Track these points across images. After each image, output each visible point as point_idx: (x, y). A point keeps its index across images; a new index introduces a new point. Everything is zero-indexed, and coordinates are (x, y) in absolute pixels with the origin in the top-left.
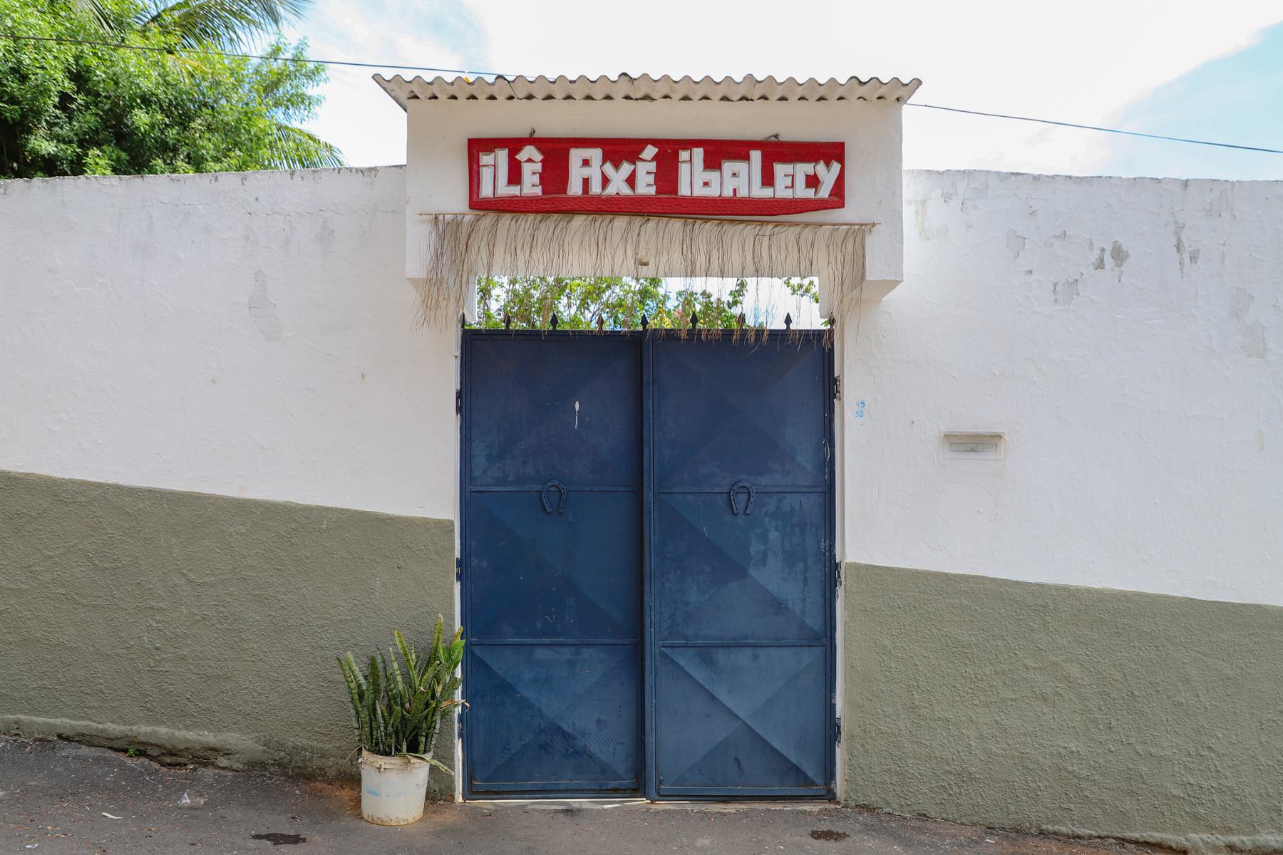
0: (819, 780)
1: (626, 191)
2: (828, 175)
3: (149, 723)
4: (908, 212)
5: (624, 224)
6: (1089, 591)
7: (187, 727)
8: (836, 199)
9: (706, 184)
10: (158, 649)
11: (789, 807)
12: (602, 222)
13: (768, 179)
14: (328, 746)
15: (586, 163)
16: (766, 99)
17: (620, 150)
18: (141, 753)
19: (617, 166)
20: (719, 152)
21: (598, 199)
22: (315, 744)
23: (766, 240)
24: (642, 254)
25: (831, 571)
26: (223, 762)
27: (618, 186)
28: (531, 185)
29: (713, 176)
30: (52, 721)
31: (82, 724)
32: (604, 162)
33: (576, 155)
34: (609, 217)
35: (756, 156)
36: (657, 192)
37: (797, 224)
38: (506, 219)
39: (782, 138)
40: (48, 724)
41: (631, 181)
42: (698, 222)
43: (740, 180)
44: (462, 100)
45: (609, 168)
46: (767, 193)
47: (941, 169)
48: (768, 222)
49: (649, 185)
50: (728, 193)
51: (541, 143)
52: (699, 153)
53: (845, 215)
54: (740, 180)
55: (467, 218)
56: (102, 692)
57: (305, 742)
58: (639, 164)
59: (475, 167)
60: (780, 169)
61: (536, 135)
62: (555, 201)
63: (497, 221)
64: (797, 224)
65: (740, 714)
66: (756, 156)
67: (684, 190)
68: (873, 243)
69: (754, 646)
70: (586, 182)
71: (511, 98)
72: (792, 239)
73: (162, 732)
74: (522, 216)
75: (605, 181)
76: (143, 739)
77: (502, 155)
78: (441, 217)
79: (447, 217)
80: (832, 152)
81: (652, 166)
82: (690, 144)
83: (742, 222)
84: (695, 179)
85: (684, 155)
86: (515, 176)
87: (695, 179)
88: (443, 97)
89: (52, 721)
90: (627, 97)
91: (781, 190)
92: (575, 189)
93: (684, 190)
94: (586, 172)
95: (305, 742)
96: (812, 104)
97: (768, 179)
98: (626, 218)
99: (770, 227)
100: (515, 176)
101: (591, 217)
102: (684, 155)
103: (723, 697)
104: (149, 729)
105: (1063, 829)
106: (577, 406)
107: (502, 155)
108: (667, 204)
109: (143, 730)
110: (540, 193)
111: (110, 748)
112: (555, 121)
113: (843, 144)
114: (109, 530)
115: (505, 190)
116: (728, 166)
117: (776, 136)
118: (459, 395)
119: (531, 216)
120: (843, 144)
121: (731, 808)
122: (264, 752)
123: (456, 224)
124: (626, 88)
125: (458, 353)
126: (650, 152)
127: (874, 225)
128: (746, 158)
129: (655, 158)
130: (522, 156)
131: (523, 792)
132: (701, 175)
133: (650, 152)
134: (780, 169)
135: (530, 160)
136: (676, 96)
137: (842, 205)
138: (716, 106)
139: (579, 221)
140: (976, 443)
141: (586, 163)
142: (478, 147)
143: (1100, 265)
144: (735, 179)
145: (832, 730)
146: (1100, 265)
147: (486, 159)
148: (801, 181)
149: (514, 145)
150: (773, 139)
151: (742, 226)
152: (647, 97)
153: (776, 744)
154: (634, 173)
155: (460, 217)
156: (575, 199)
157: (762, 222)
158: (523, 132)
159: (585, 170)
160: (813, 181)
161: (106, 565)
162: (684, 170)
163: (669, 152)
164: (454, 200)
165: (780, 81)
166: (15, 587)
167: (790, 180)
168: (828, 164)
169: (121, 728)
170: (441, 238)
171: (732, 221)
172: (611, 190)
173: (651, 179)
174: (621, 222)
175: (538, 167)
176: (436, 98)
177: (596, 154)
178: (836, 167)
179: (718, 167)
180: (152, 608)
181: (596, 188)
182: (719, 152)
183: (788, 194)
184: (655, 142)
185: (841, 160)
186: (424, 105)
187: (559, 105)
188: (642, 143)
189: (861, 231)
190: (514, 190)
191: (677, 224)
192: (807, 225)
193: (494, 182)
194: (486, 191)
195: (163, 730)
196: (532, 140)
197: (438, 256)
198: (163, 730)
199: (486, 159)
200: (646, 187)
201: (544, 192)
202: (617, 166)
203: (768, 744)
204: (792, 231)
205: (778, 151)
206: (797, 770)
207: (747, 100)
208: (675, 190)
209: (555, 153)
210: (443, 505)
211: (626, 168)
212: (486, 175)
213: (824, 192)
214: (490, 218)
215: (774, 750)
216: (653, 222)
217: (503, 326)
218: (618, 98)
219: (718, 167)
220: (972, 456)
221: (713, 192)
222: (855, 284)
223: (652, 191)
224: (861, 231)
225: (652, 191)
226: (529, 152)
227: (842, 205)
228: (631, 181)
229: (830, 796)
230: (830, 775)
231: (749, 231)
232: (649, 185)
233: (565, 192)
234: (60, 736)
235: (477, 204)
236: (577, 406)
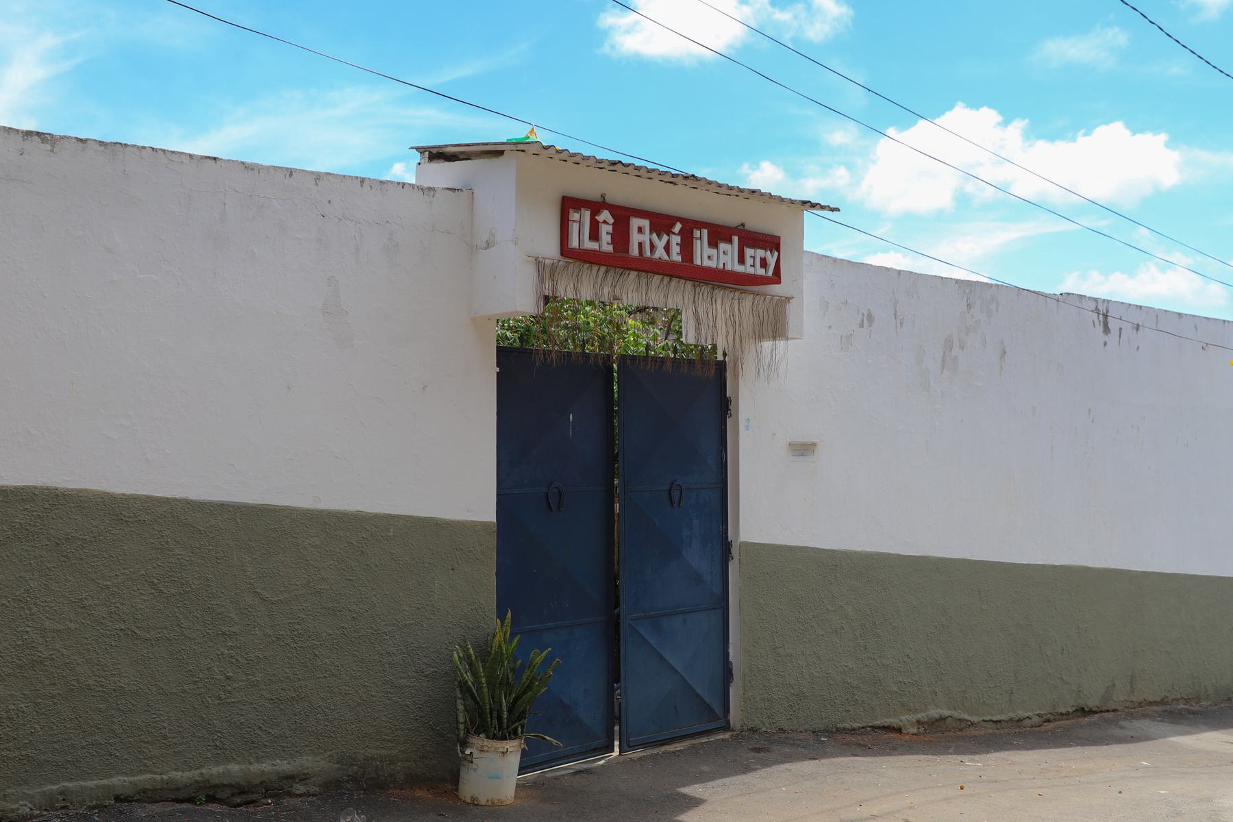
0: (721, 715)
3: (217, 763)
6: (855, 552)
7: (258, 760)
10: (228, 678)
11: (704, 740)
13: (742, 260)
14: (394, 752)
18: (211, 799)
20: (719, 234)
22: (383, 752)
24: (617, 292)
25: (726, 547)
26: (300, 788)
27: (660, 253)
28: (606, 244)
29: (713, 252)
30: (105, 782)
31: (144, 779)
33: (635, 223)
39: (749, 227)
40: (104, 787)
41: (667, 248)
44: (570, 164)
48: (736, 289)
50: (721, 266)
53: (775, 289)
56: (165, 737)
57: (374, 751)
60: (749, 252)
62: (620, 260)
65: (679, 669)
66: (736, 239)
69: (683, 613)
73: (235, 769)
76: (217, 782)
82: (700, 225)
83: (725, 288)
84: (706, 256)
86: (595, 235)
89: (105, 782)
93: (698, 262)
94: (641, 238)
95: (374, 751)
97: (742, 260)
100: (595, 235)
102: (697, 233)
103: (668, 657)
104: (221, 769)
105: (848, 726)
107: (587, 214)
109: (214, 771)
111: (173, 800)
112: (621, 192)
114: (177, 551)
117: (743, 225)
121: (678, 746)
122: (339, 769)
126: (678, 227)
130: (600, 218)
131: (535, 765)
133: (678, 227)
135: (605, 222)
140: (803, 449)
142: (569, 204)
143: (862, 326)
145: (727, 674)
146: (862, 326)
147: (575, 216)
149: (596, 207)
153: (699, 691)
156: (633, 259)
159: (640, 235)
160: (764, 263)
161: (173, 591)
162: (697, 244)
164: (549, 248)
166: (61, 627)
169: (187, 774)
175: (610, 228)
177: (646, 223)
180: (223, 634)
182: (719, 234)
183: (751, 271)
184: (681, 220)
185: (779, 251)
193: (579, 238)
195: (234, 767)
198: (234, 767)
199: (575, 216)
203: (693, 690)
206: (709, 708)
208: (627, 251)
210: (487, 512)
212: (574, 228)
214: (574, 266)
215: (698, 696)
216: (674, 281)
217: (517, 344)
220: (801, 458)
226: (605, 215)
229: (727, 727)
230: (726, 709)
234: (118, 799)
235: (565, 250)
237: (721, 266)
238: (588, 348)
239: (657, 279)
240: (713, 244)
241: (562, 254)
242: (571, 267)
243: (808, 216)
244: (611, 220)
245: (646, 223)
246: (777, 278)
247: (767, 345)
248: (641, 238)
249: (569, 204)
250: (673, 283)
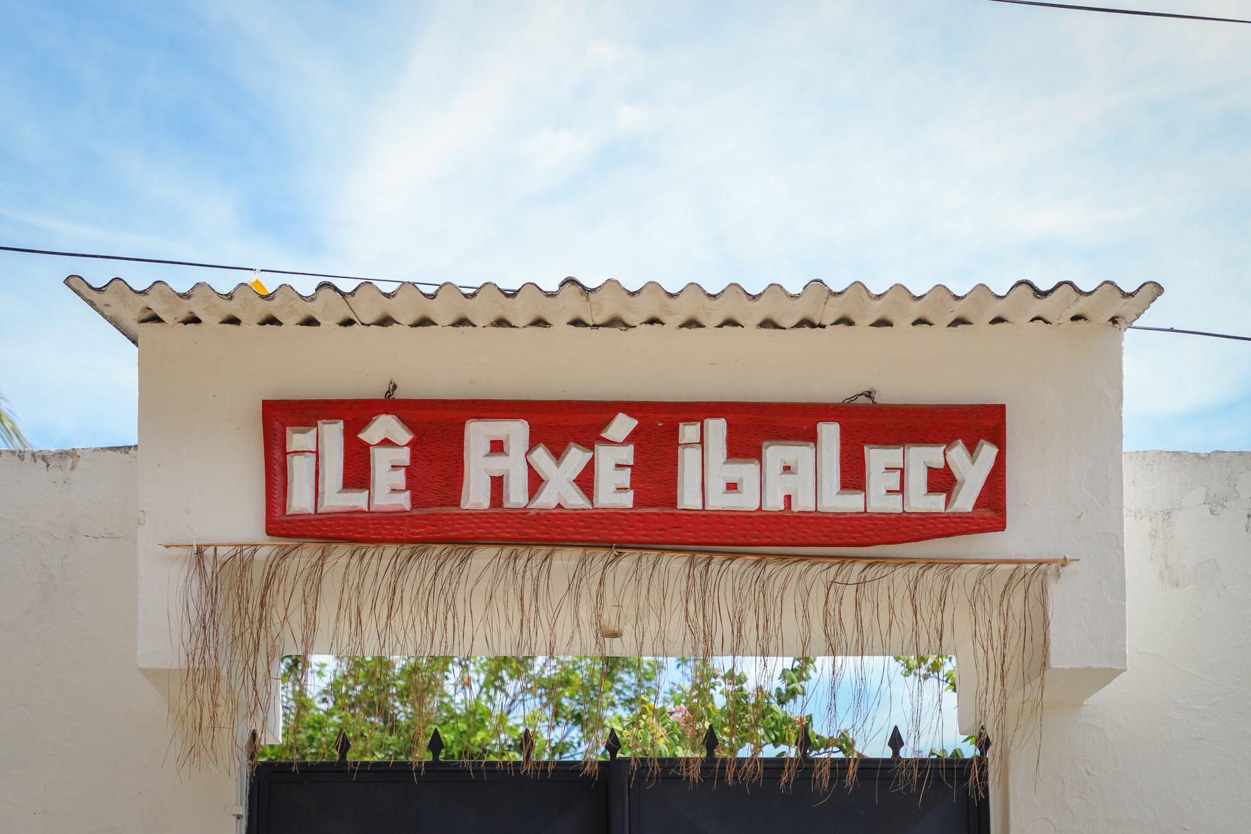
13: (853, 477)
20: (758, 426)
29: (745, 471)
35: (830, 433)
41: (586, 481)
50: (775, 503)
60: (878, 459)
62: (437, 520)
66: (830, 433)
80: (982, 424)
82: (699, 411)
84: (709, 477)
86: (357, 472)
91: (879, 498)
94: (497, 465)
97: (853, 477)
100: (357, 472)
102: (688, 432)
107: (333, 433)
112: (436, 367)
126: (622, 426)
130: (372, 434)
133: (622, 426)
135: (386, 443)
142: (282, 417)
149: (355, 414)
160: (942, 480)
162: (689, 460)
164: (237, 517)
167: (897, 479)
175: (404, 456)
177: (516, 431)
178: (988, 452)
184: (630, 408)
185: (998, 439)
193: (316, 482)
199: (299, 440)
212: (300, 469)
213: (965, 501)
214: (307, 553)
224: (1037, 573)
226: (384, 427)
235: (281, 524)
237: (780, 505)
238: (308, 759)
239: (566, 560)
241: (271, 531)
243: (944, 496)
244: (403, 436)
246: (993, 509)
248: (497, 465)
249: (282, 417)
250: (714, 566)
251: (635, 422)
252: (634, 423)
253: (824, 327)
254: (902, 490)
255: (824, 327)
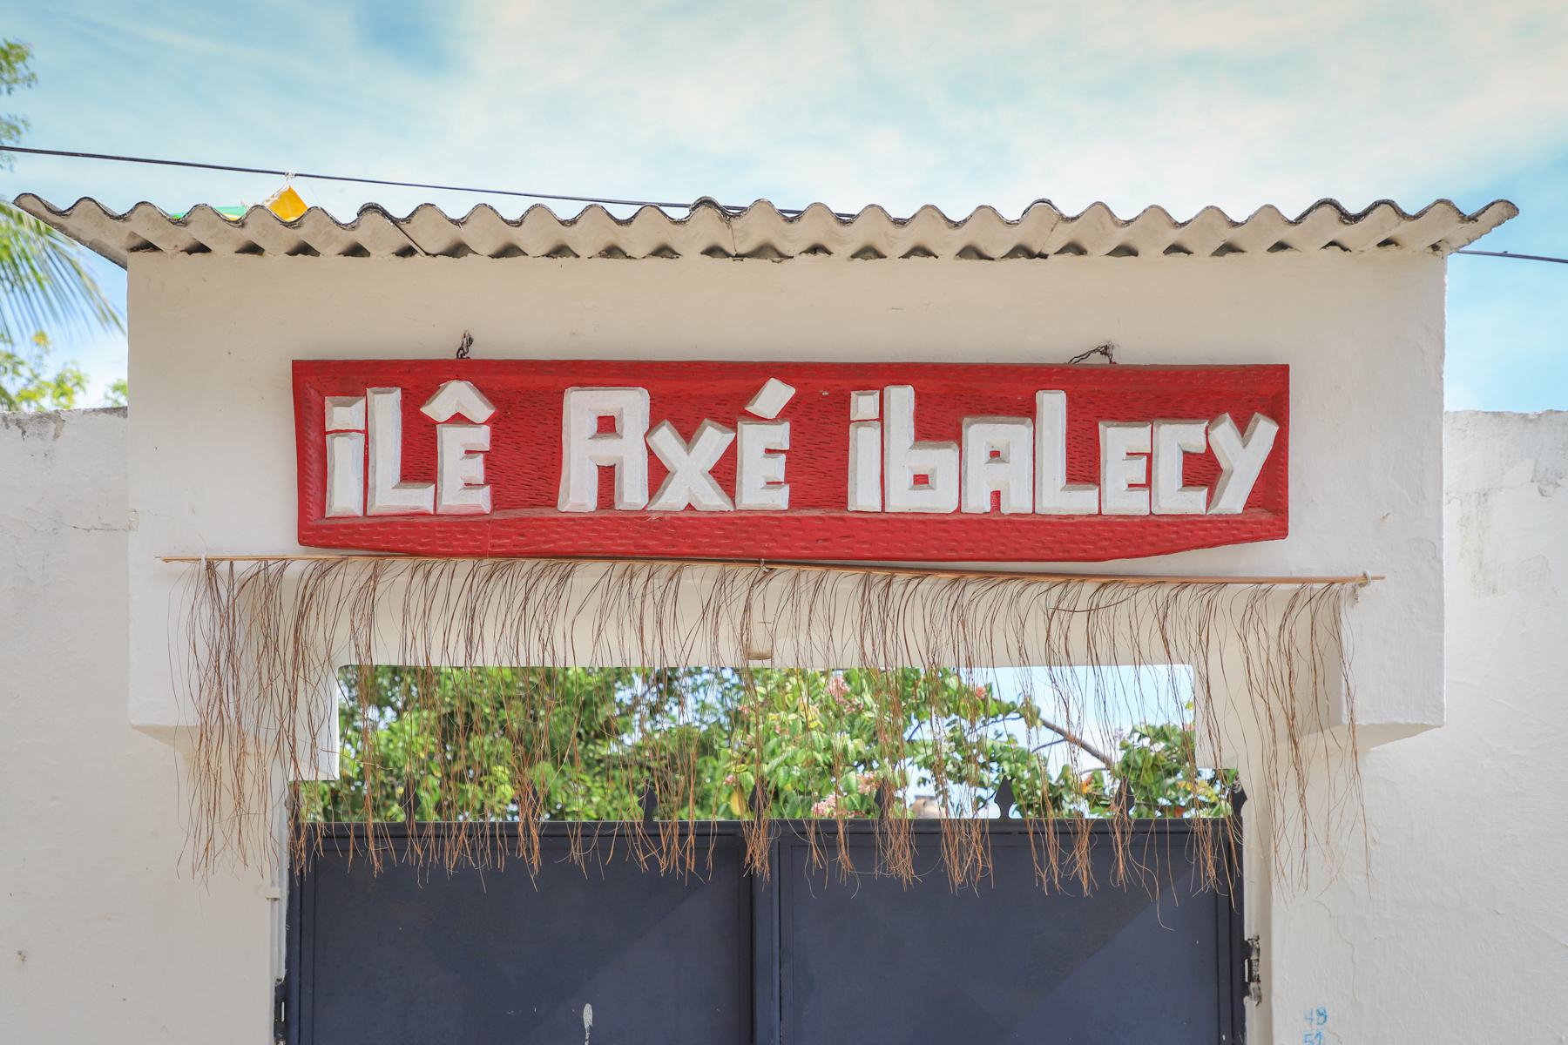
1: (712, 499)
2: (1242, 454)
4: (1451, 537)
5: (708, 583)
8: (1265, 516)
9: (921, 480)
12: (650, 579)
13: (1084, 465)
15: (607, 425)
16: (1080, 251)
17: (696, 392)
19: (688, 435)
20: (955, 396)
21: (639, 521)
23: (1079, 621)
27: (691, 487)
28: (462, 485)
29: (939, 459)
32: (654, 423)
34: (669, 567)
35: (1053, 405)
36: (792, 502)
37: (1160, 581)
38: (399, 571)
39: (1128, 354)
41: (725, 472)
42: (901, 577)
43: (1010, 469)
44: (276, 258)
45: (666, 440)
46: (1081, 502)
47: (1533, 408)
48: (1084, 577)
49: (772, 484)
50: (978, 503)
51: (490, 376)
52: (902, 399)
54: (1010, 469)
55: (294, 569)
58: (747, 430)
59: (313, 435)
60: (1117, 440)
61: (475, 353)
62: (524, 525)
63: (374, 577)
64: (1160, 581)
66: (1053, 405)
67: (863, 497)
68: (1361, 624)
70: (607, 476)
71: (407, 252)
72: (1149, 623)
74: (438, 565)
75: (658, 473)
77: (386, 406)
78: (223, 568)
79: (240, 567)
80: (1258, 392)
81: (781, 435)
82: (878, 375)
84: (891, 467)
85: (863, 405)
86: (420, 461)
87: (891, 467)
88: (224, 249)
90: (713, 251)
91: (1118, 495)
92: (577, 493)
94: (607, 450)
96: (1202, 266)
97: (1084, 465)
98: (714, 569)
99: (1089, 587)
100: (420, 461)
101: (620, 566)
102: (863, 405)
106: (588, 1014)
107: (386, 406)
108: (821, 532)
110: (486, 507)
112: (527, 317)
113: (1284, 370)
115: (395, 497)
116: (980, 434)
117: (1105, 351)
118: (283, 993)
119: (464, 565)
120: (1284, 370)
123: (266, 579)
124: (710, 229)
125: (282, 892)
126: (774, 396)
127: (1365, 580)
128: (1028, 410)
129: (787, 413)
130: (438, 408)
132: (908, 456)
133: (774, 396)
134: (1117, 440)
135: (459, 419)
136: (843, 251)
137: (1278, 529)
138: (947, 271)
139: (589, 574)
141: (607, 425)
142: (319, 383)
144: (998, 468)
147: (341, 414)
148: (1170, 469)
149: (416, 379)
150: (1097, 360)
151: (1014, 587)
152: (764, 251)
154: (734, 443)
155: (273, 568)
156: (579, 522)
157: (1069, 576)
158: (438, 344)
159: (605, 447)
160: (1202, 470)
162: (863, 444)
163: (825, 397)
164: (261, 521)
165: (1123, 216)
167: (1143, 468)
168: (1242, 425)
170: (227, 618)
171: (988, 574)
172: (673, 499)
173: (777, 468)
174: (698, 579)
175: (481, 437)
176: (203, 249)
177: (633, 404)
178: (1265, 430)
179: (954, 436)
181: (633, 494)
182: (955, 396)
183: (1136, 504)
185: (1278, 411)
186: (175, 268)
187: (532, 272)
188: (754, 374)
189: (1330, 594)
190: (418, 498)
191: (845, 583)
192: (1185, 583)
194: (344, 499)
196: (463, 367)
197: (225, 659)
199: (341, 414)
200: (764, 487)
201: (497, 501)
202: (688, 435)
204: (1146, 600)
205: (1109, 393)
207: (1030, 255)
208: (841, 500)
209: (526, 397)
211: (713, 440)
212: (343, 456)
213: (1233, 499)
214: (354, 570)
216: (782, 577)
218: (691, 253)
219: (954, 436)
221: (939, 500)
222: (1309, 702)
223: (780, 499)
224: (1330, 594)
225: (780, 499)
227: (1278, 529)
228: (725, 472)
231: (1034, 599)
232: (772, 484)
233: (552, 502)
235: (317, 528)
236: (588, 1014)
240: (937, 425)
241: (304, 540)
242: (803, 577)
244: (481, 410)
245: (633, 404)
246: (1270, 506)
247: (182, 723)
248: (607, 450)
249: (319, 383)
250: (897, 587)
251: (792, 391)
252: (789, 392)
253: (1045, 256)
254: (1148, 484)
255: (1045, 256)
